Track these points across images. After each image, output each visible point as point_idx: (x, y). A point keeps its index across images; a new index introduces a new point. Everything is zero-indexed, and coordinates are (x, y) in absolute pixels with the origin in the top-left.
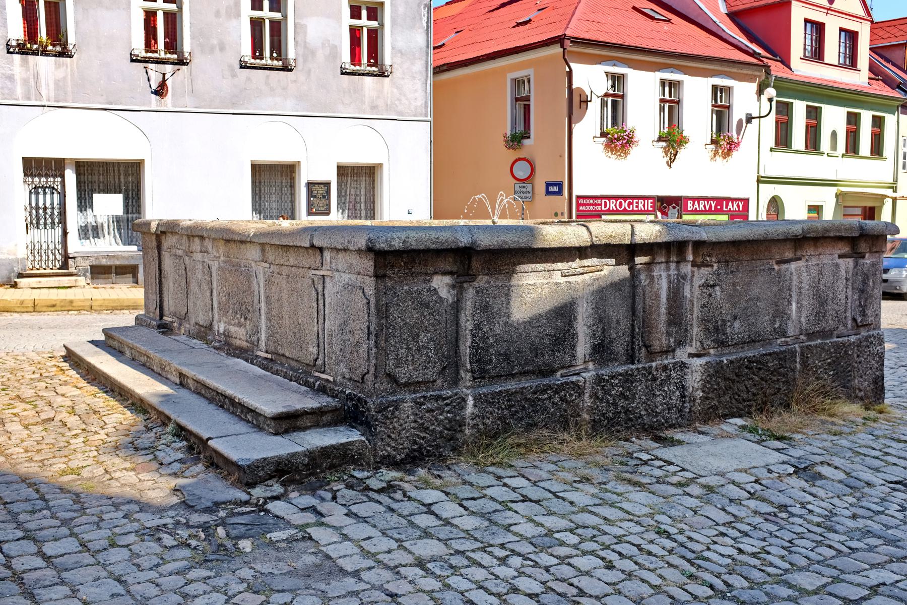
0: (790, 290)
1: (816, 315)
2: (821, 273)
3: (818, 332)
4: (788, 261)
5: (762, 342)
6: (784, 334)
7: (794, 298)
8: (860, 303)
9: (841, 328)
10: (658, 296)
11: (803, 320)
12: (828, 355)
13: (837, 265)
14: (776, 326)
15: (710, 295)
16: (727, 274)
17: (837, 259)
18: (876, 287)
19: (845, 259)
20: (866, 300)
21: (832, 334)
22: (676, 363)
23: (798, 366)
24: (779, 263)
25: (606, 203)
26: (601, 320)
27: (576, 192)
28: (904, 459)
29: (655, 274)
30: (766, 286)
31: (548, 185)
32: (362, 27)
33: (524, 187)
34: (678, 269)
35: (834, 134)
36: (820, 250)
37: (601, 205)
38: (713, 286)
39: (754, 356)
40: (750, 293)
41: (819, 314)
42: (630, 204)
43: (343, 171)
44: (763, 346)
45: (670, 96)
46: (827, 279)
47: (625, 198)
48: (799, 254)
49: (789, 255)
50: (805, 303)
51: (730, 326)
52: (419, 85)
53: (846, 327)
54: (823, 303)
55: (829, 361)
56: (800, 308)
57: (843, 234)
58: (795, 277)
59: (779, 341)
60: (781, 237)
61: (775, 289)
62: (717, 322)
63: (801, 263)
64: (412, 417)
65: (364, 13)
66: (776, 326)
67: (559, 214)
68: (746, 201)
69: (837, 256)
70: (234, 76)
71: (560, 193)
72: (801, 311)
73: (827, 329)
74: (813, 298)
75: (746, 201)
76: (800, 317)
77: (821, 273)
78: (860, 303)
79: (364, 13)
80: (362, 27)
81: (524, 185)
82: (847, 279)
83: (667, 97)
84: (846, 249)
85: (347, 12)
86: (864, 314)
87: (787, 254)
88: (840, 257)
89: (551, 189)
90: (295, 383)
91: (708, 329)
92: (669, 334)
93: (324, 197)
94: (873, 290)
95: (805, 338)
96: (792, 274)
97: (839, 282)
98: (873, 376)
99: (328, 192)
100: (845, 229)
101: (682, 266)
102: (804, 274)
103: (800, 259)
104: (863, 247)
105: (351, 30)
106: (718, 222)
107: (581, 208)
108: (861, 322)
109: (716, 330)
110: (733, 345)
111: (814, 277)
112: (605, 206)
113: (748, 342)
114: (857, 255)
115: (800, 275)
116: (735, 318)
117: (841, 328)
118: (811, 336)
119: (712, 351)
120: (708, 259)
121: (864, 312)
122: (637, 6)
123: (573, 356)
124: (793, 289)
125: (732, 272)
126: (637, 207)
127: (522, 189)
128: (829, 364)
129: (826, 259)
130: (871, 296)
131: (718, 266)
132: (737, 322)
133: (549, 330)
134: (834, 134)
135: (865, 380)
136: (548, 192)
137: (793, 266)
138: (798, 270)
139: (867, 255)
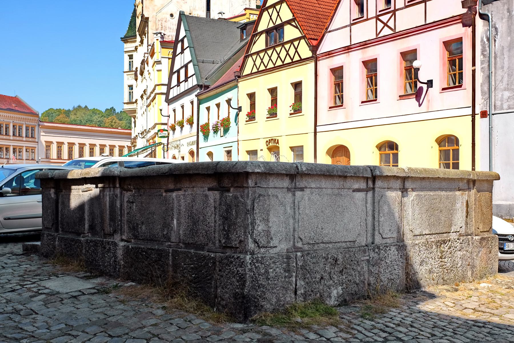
0: (172, 210)
1: (190, 231)
2: (194, 200)
3: (192, 243)
4: (172, 191)
5: (158, 242)
6: (169, 239)
7: (175, 216)
8: (224, 227)
9: (210, 245)
10: (106, 204)
11: (181, 232)
12: (191, 261)
13: (206, 196)
14: (165, 233)
15: (131, 208)
16: (138, 196)
17: (207, 191)
18: (239, 216)
19: (214, 192)
20: (229, 227)
21: (203, 248)
22: (112, 242)
23: (171, 263)
24: (167, 191)
26: (92, 213)
29: (105, 193)
30: (158, 206)
34: (114, 191)
36: (194, 184)
38: (133, 202)
39: (144, 248)
40: (150, 209)
41: (193, 230)
44: (158, 244)
46: (198, 205)
48: (178, 186)
49: (171, 186)
50: (183, 221)
51: (141, 227)
53: (215, 245)
54: (195, 223)
55: (192, 266)
56: (179, 224)
57: (200, 172)
58: (176, 202)
59: (167, 244)
60: (155, 174)
61: (164, 208)
62: (134, 224)
63: (181, 193)
64: (481, 262)
66: (165, 233)
69: (207, 188)
72: (180, 226)
73: (199, 243)
74: (188, 218)
76: (179, 230)
77: (194, 200)
78: (224, 227)
82: (215, 208)
84: (214, 184)
86: (228, 238)
87: (170, 186)
88: (210, 189)
91: (130, 227)
92: (110, 226)
94: (236, 219)
95: (183, 246)
96: (173, 199)
97: (208, 209)
98: (234, 291)
100: (202, 168)
101: (116, 190)
102: (182, 201)
103: (180, 190)
104: (226, 183)
106: (136, 163)
108: (224, 243)
109: (134, 228)
110: (142, 240)
111: (189, 204)
113: (149, 240)
114: (223, 190)
115: (179, 201)
116: (143, 223)
117: (210, 245)
118: (188, 245)
119: (133, 240)
120: (129, 186)
121: (228, 236)
123: (84, 229)
124: (175, 210)
125: (141, 195)
128: (192, 268)
129: (199, 191)
130: (235, 224)
131: (135, 191)
132: (144, 226)
133: (78, 215)
135: (226, 292)
137: (174, 194)
138: (178, 197)
139: (232, 189)
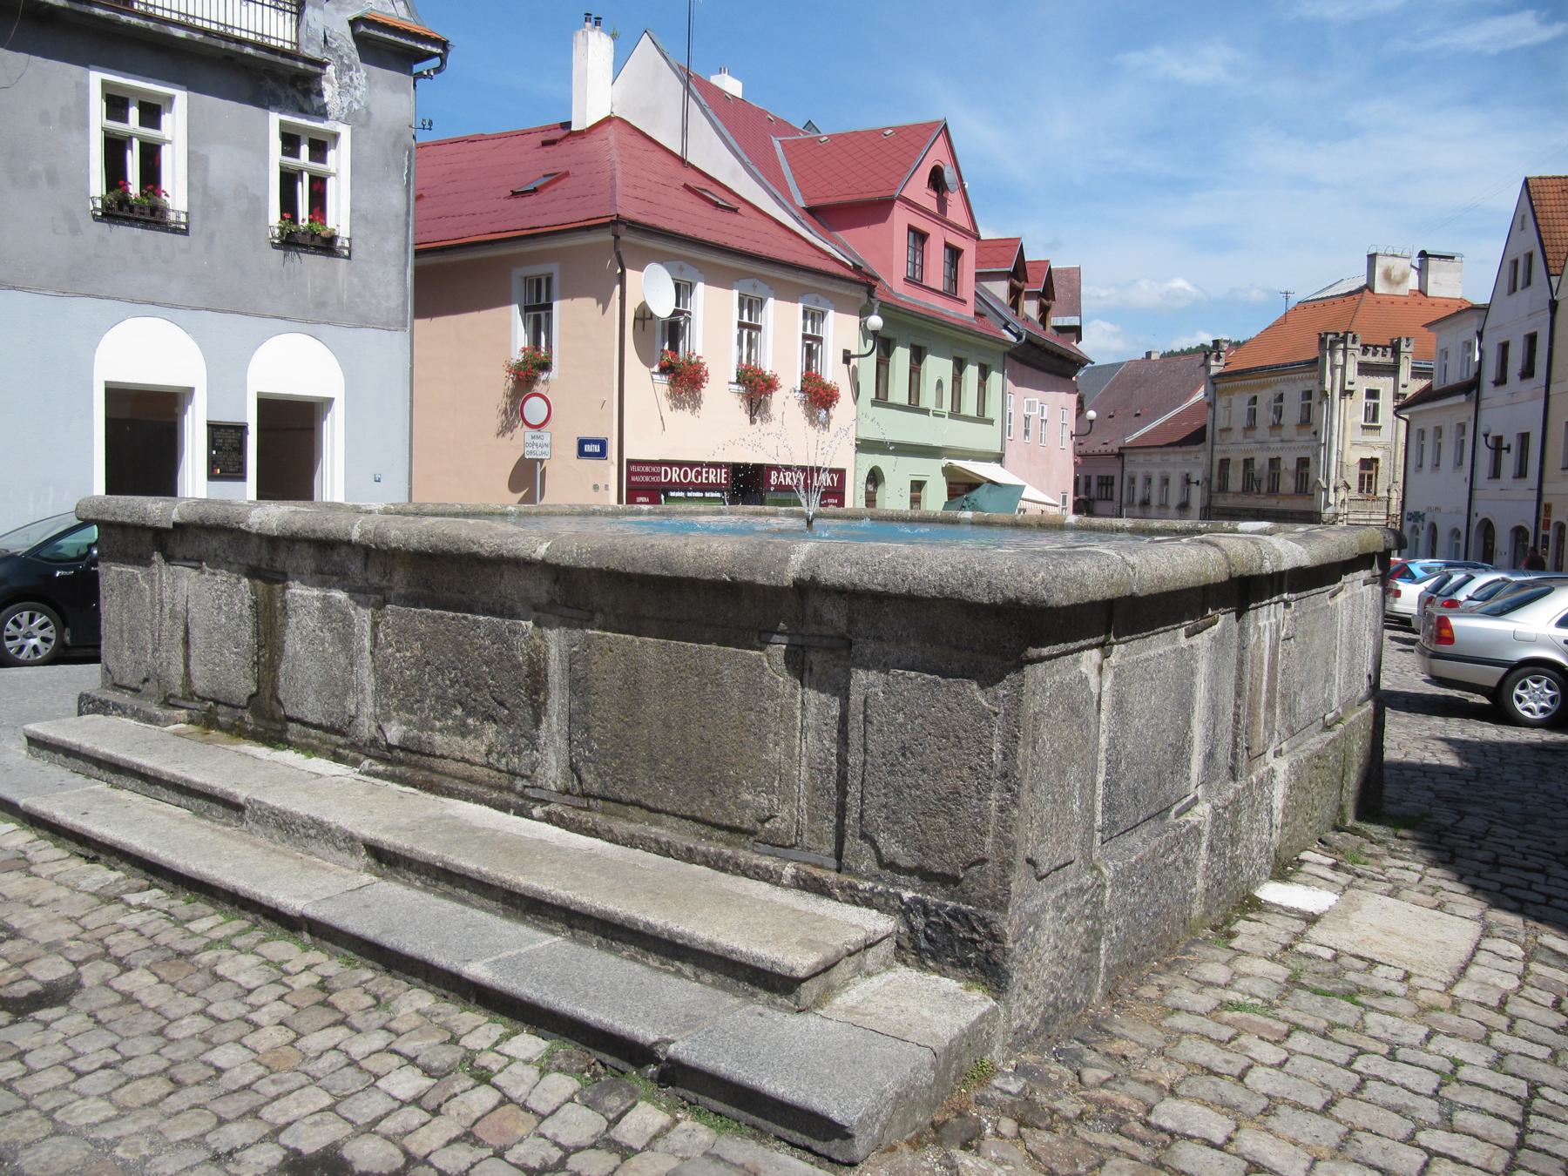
25: (666, 471)
27: (627, 455)
28: (1566, 900)
31: (582, 443)
32: (130, 138)
33: (539, 437)
35: (940, 384)
37: (660, 474)
42: (699, 474)
43: (270, 407)
45: (750, 319)
47: (692, 465)
52: (392, 274)
65: (134, 113)
67: (602, 487)
68: (841, 473)
70: (75, 231)
71: (602, 454)
75: (841, 473)
79: (134, 113)
80: (130, 138)
81: (538, 434)
83: (746, 319)
85: (275, 144)
89: (588, 448)
90: (702, 868)
93: (235, 449)
99: (241, 449)
105: (282, 174)
107: (633, 479)
112: (666, 477)
122: (691, 184)
126: (707, 478)
127: (536, 441)
134: (940, 384)
136: (582, 453)
